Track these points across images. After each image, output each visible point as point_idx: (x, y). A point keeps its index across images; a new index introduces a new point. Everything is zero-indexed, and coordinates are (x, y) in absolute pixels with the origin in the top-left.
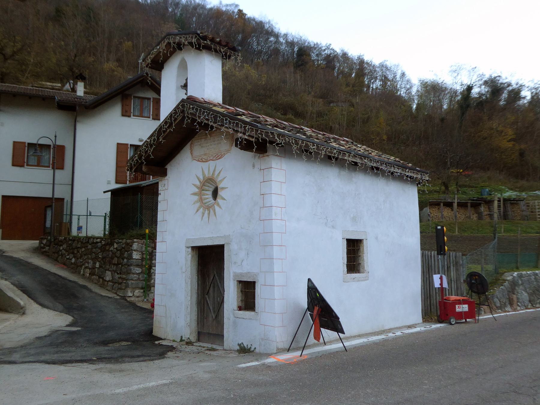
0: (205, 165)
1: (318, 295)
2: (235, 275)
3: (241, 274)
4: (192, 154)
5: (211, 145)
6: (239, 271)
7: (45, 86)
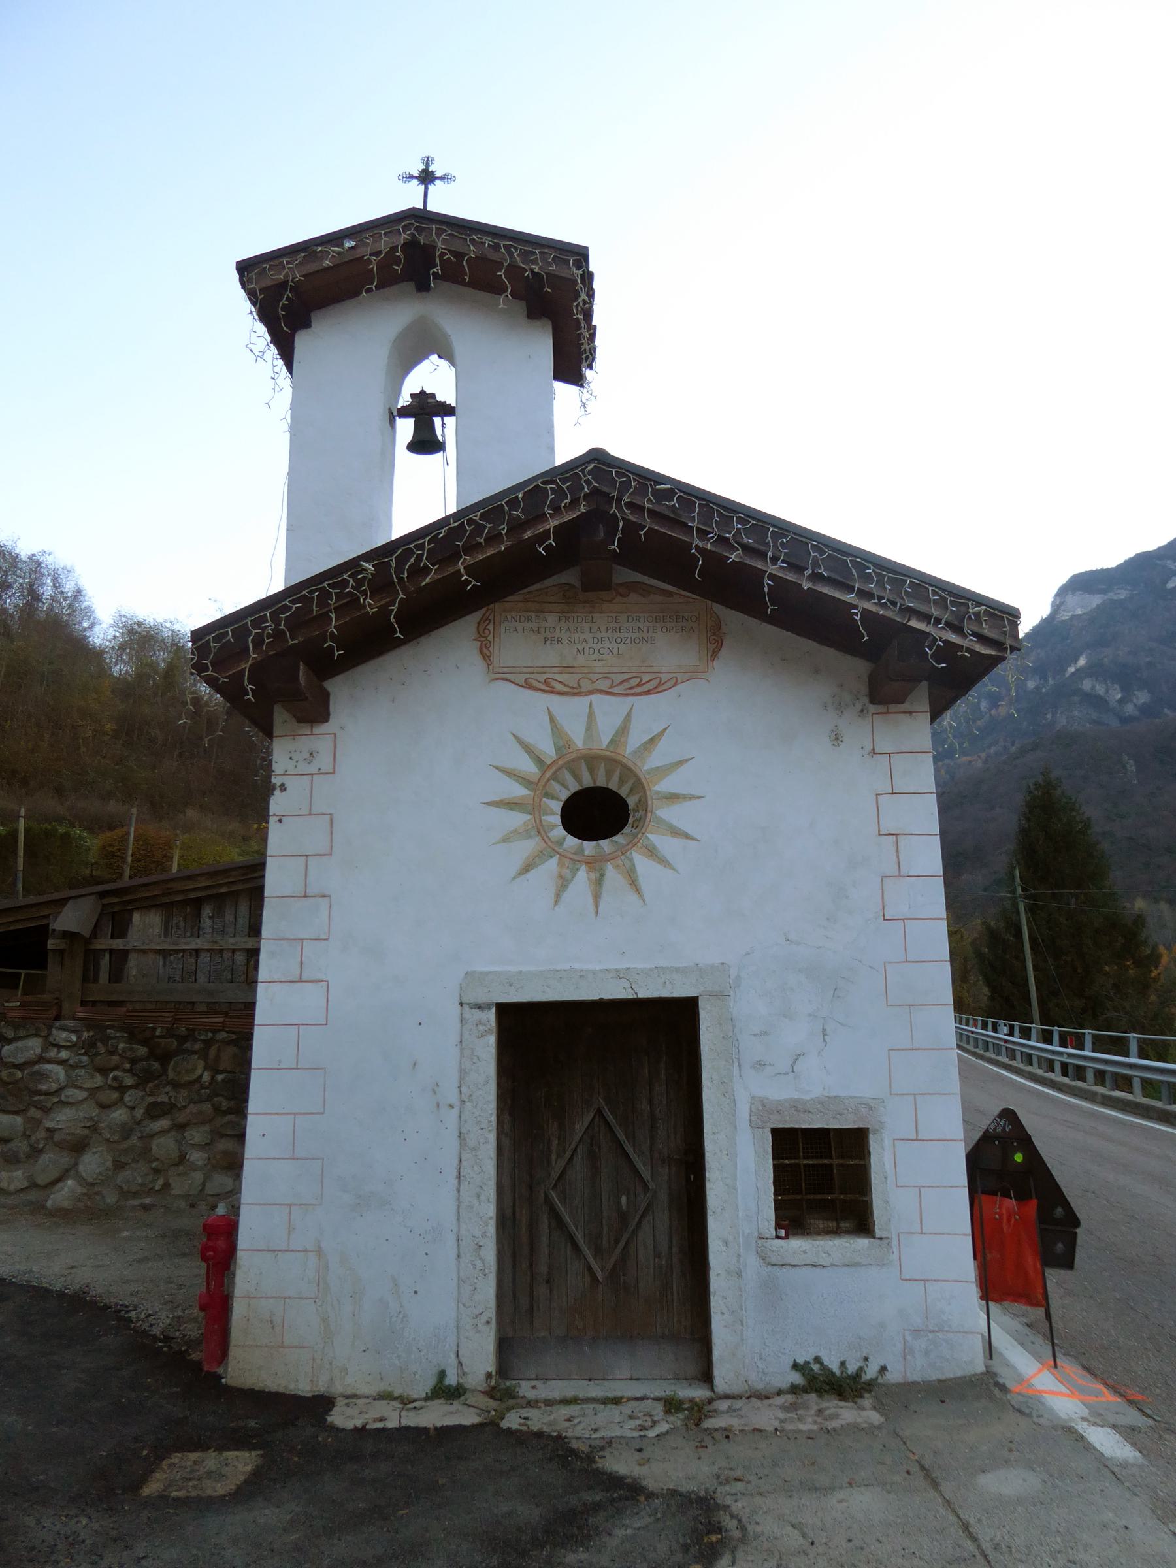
2: (762, 1108)
3: (796, 1106)
6: (779, 1092)
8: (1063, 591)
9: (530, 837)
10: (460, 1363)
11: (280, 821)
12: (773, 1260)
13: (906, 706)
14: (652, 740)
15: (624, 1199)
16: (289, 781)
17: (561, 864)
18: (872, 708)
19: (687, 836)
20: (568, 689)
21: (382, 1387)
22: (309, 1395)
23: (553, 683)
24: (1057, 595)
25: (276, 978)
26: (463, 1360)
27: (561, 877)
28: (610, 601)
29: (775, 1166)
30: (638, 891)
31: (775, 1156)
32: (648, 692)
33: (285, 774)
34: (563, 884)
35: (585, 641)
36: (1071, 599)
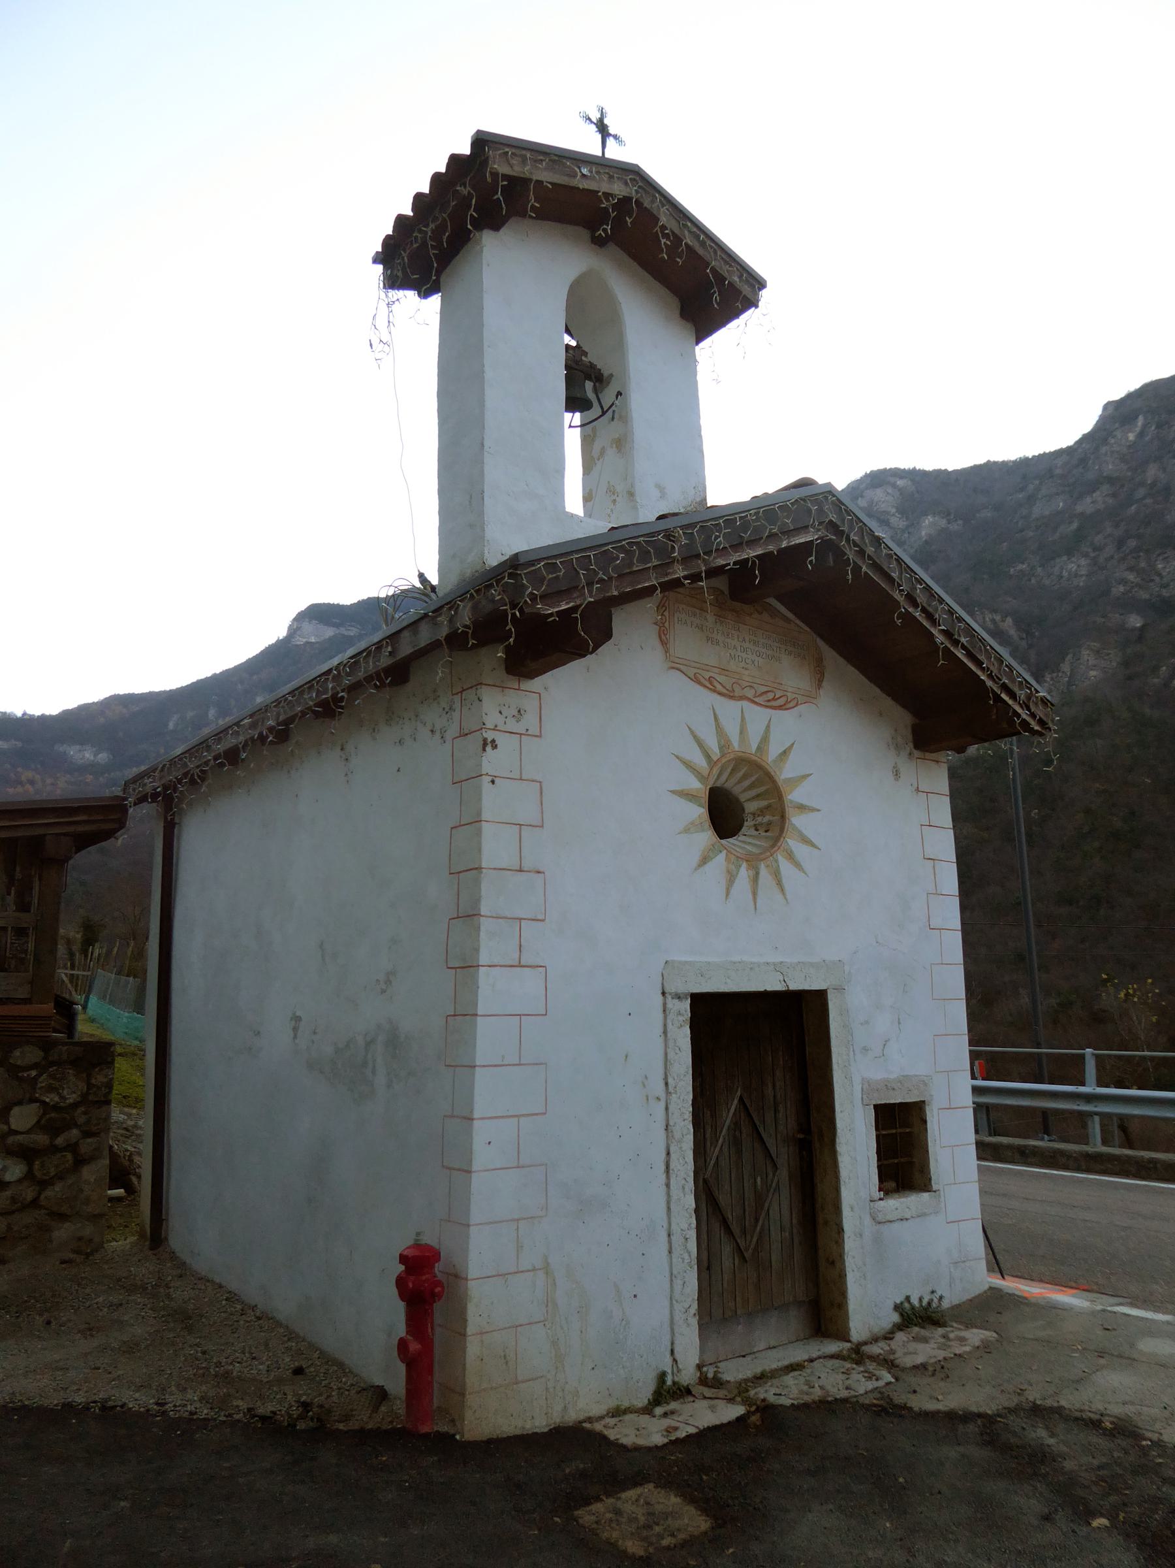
0: (730, 711)
1: (900, 483)
2: (869, 1087)
3: (888, 1086)
4: (664, 643)
5: (745, 650)
6: (877, 1075)
7: (991, 1256)
8: (301, 617)
9: (703, 831)
10: (675, 1360)
11: (493, 782)
12: (880, 1217)
13: (934, 756)
14: (785, 752)
15: (759, 1179)
16: (501, 739)
17: (727, 859)
18: (917, 753)
19: (813, 845)
20: (725, 691)
21: (612, 1403)
22: (546, 1430)
23: (716, 684)
24: (294, 620)
25: (496, 962)
26: (677, 1356)
27: (728, 872)
28: (750, 615)
29: (878, 1137)
30: (782, 890)
31: (877, 1129)
32: (780, 708)
33: (495, 729)
34: (731, 879)
35: (735, 647)
36: (308, 627)
